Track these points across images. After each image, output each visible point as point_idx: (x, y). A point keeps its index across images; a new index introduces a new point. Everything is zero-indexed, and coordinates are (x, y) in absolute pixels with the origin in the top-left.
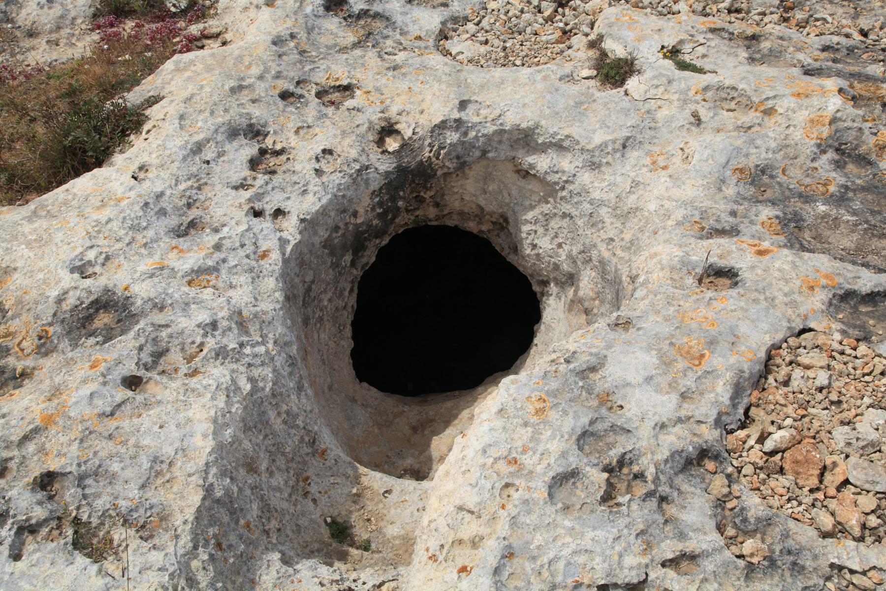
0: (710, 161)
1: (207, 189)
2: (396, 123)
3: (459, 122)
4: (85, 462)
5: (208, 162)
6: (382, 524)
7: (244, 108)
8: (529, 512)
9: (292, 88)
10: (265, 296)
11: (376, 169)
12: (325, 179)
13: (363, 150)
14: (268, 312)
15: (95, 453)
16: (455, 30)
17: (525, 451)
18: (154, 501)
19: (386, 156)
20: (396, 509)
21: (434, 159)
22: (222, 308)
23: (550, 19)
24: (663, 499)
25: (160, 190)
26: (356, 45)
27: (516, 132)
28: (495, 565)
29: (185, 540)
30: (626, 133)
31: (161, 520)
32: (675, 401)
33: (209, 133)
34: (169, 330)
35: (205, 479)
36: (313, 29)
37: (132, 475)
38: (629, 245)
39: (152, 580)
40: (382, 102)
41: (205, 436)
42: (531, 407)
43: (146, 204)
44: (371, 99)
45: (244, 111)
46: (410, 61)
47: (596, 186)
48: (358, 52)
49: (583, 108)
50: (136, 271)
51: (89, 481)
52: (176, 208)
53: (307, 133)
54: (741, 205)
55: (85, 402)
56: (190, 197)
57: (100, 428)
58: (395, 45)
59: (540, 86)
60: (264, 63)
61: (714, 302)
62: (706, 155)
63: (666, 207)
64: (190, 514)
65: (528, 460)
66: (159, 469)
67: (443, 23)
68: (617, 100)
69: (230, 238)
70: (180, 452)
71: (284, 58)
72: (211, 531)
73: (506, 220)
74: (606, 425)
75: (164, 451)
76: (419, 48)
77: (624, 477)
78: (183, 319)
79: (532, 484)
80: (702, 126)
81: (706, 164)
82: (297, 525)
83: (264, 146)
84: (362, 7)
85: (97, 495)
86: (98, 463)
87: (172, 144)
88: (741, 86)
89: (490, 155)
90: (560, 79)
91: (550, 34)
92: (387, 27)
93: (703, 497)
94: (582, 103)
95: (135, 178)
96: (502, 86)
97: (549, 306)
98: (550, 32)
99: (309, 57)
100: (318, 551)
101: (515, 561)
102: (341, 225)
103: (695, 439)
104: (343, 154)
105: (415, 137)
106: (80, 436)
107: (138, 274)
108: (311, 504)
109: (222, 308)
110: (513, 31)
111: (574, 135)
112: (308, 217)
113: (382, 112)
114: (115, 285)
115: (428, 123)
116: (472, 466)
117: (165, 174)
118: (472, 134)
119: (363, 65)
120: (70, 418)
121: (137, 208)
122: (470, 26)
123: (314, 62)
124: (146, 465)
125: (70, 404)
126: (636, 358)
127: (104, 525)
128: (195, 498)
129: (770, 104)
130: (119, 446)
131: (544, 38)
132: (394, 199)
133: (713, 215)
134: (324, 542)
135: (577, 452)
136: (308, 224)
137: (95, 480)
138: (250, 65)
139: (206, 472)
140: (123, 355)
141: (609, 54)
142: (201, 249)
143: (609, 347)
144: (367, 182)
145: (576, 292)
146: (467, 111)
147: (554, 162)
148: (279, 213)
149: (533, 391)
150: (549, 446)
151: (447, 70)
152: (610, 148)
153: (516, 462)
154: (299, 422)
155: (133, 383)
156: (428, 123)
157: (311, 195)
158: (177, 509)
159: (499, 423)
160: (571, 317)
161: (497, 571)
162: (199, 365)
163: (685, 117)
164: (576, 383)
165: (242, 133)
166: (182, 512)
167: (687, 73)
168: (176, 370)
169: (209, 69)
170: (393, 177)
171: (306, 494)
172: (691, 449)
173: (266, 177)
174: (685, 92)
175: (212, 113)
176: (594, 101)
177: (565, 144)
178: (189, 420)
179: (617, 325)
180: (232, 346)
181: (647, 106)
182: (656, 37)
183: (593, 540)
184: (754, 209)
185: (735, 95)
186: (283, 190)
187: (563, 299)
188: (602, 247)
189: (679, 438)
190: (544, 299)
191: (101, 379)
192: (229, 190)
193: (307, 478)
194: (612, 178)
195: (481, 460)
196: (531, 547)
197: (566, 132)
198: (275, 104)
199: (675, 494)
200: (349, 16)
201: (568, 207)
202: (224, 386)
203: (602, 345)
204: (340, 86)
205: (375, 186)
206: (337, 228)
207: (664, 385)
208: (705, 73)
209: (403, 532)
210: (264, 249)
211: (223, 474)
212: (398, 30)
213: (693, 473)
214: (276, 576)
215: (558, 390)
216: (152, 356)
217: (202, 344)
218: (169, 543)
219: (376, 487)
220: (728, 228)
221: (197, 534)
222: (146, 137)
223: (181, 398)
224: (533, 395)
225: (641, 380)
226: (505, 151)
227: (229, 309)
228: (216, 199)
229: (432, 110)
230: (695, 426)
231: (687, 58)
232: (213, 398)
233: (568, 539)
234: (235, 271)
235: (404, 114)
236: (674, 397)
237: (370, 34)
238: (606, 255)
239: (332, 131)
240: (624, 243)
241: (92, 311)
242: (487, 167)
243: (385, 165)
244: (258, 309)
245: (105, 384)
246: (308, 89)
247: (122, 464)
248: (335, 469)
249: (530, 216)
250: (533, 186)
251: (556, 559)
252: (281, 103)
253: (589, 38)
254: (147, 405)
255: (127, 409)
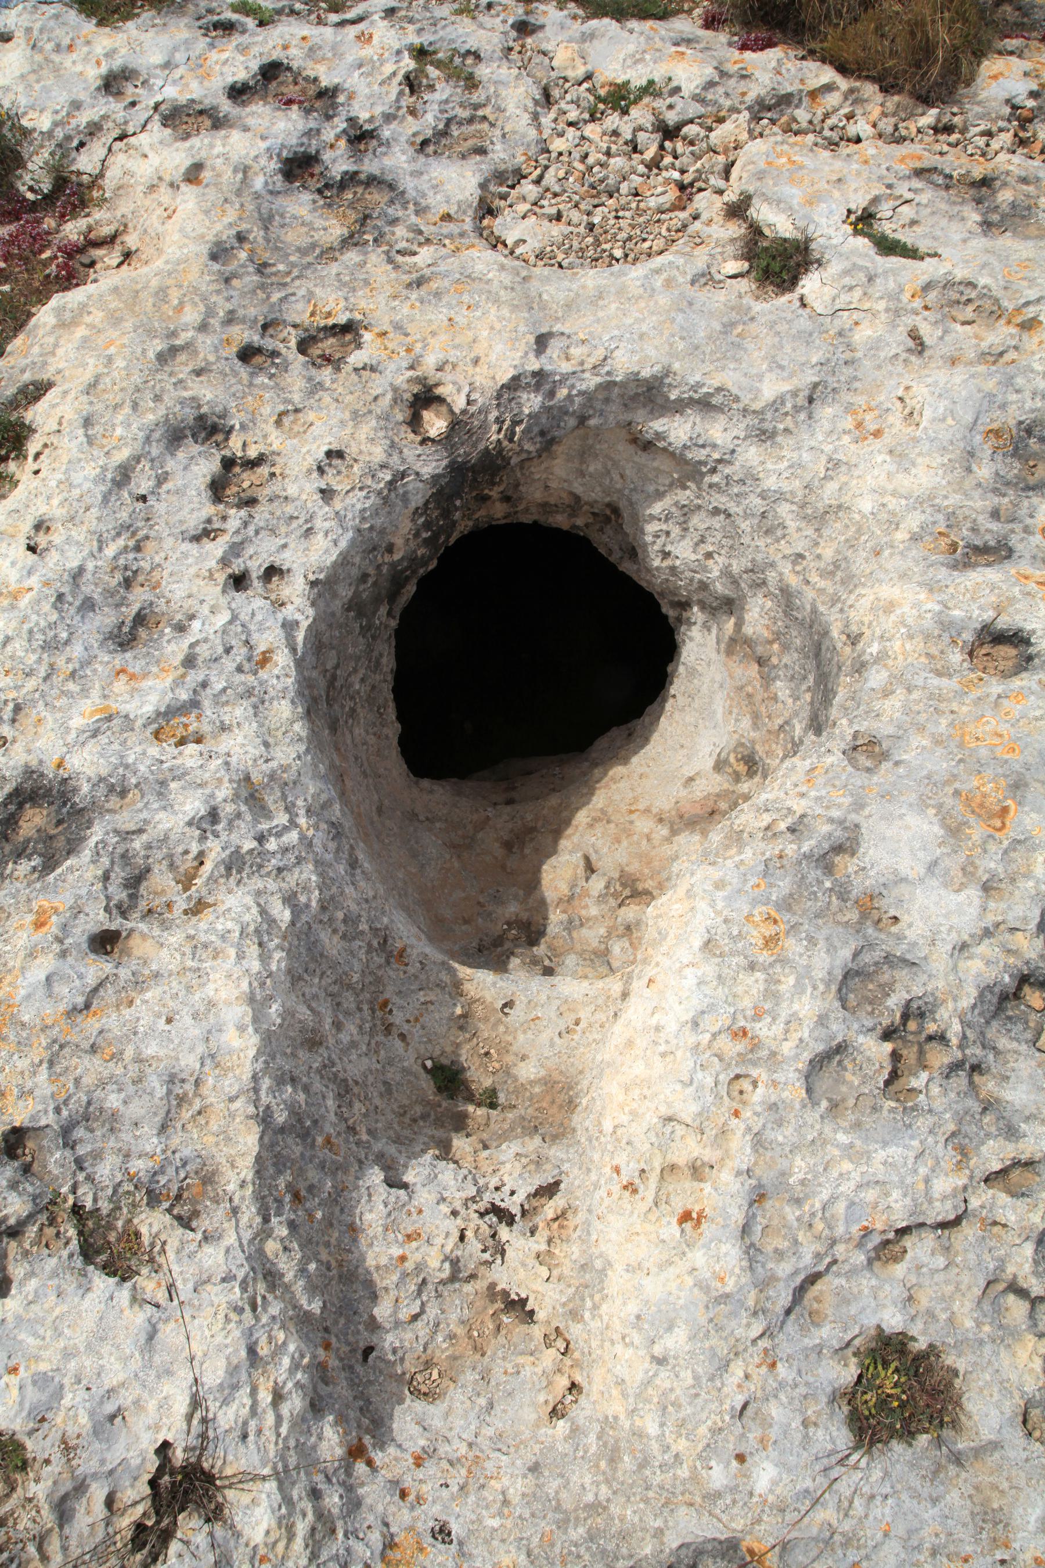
0: (950, 421)
1: (150, 546)
2: (437, 385)
3: (540, 375)
4: (66, 1102)
5: (143, 498)
6: (509, 1059)
7: (185, 389)
8: (780, 1123)
9: (256, 339)
10: (279, 734)
11: (417, 474)
12: (338, 504)
13: (393, 445)
14: (289, 766)
15: (77, 1081)
16: (504, 197)
17: (757, 1016)
18: (186, 1152)
19: (429, 448)
20: (525, 1032)
21: (505, 443)
22: (220, 780)
23: (654, 165)
24: (976, 1068)
25: (75, 564)
26: (349, 241)
27: (633, 385)
28: (741, 1222)
29: (249, 1214)
30: (810, 377)
31: (204, 1183)
32: (977, 902)
33: (138, 445)
34: (144, 837)
35: (256, 1103)
36: (271, 218)
37: (143, 1111)
38: (831, 568)
39: (216, 1301)
40: (409, 350)
41: (241, 1029)
42: (755, 933)
43: (60, 597)
44: (391, 346)
45: (186, 394)
46: (442, 268)
47: (772, 468)
48: (352, 256)
49: (735, 332)
50: (68, 730)
51: (79, 1133)
52: (109, 593)
53: (294, 422)
54: (1004, 495)
55: (41, 993)
56: (126, 568)
57: (74, 1038)
58: (411, 235)
59: (663, 300)
60: (204, 299)
61: (1005, 702)
62: (941, 410)
63: (890, 507)
64: (246, 1169)
65: (763, 1029)
66: (180, 1097)
67: (483, 186)
68: (789, 316)
69: (206, 640)
70: (208, 1061)
71: (235, 282)
72: (282, 1183)
73: (616, 510)
74: (878, 954)
75: (183, 1063)
76: (450, 236)
77: (910, 1037)
78: (162, 815)
79: (779, 1077)
80: (926, 354)
81: (943, 426)
82: (385, 1083)
83: (227, 453)
84: (345, 168)
85: (97, 1156)
86: (85, 1099)
87: (81, 474)
88: (982, 281)
89: (592, 422)
90: (693, 283)
91: (660, 194)
92: (392, 202)
93: (1033, 1057)
94: (733, 324)
95: (32, 549)
96: (601, 303)
97: (691, 639)
98: (660, 189)
99: (275, 274)
100: (424, 1117)
101: (768, 1204)
102: (371, 571)
103: (1011, 960)
104: (361, 458)
105: (473, 409)
106: (46, 1055)
107: (73, 734)
108: (398, 1044)
109: (220, 780)
110: (601, 191)
111: (729, 385)
112: (322, 576)
113: (412, 367)
114: (41, 762)
115: (491, 384)
116: (678, 1047)
117: (79, 534)
118: (562, 393)
119: (367, 283)
120: (23, 1025)
121: (46, 607)
122: (528, 188)
123: (285, 285)
124: (160, 1091)
125: (18, 999)
126: (908, 827)
127: (120, 1208)
128: (249, 1140)
129: (1030, 312)
130: (111, 1064)
131: (652, 203)
132: (446, 513)
133: (965, 518)
134: (428, 1103)
135: (841, 1013)
136: (322, 588)
137: (87, 1128)
138: (181, 304)
139: (256, 1090)
140: (80, 897)
141: (767, 231)
142: (163, 670)
143: (859, 806)
144: (405, 498)
145: (739, 625)
146: (549, 351)
147: (698, 429)
148: (272, 572)
149: (754, 902)
150: (796, 1007)
151: (506, 278)
152: (789, 405)
153: (745, 1033)
154: (364, 926)
155: (105, 942)
156: (491, 384)
157: (320, 536)
158: (224, 1161)
159: (709, 969)
160: (731, 664)
161: (745, 1230)
162: (204, 892)
163: (897, 341)
164: (820, 882)
165: (188, 433)
166: (233, 1166)
167: (895, 261)
168: (169, 905)
169: (115, 320)
170: (443, 482)
171: (388, 1029)
172: (1007, 979)
173: (243, 513)
174: (893, 297)
175: (135, 406)
176: (752, 319)
177: (714, 401)
178: (211, 1004)
179: (855, 748)
180: (249, 844)
181: (837, 322)
182: (836, 194)
183: (885, 1163)
184: (1026, 503)
185: (973, 295)
186: (273, 531)
187: (714, 631)
188: (786, 568)
189: (988, 963)
190: (683, 628)
191: (56, 947)
192: (186, 546)
193: (385, 1003)
194: (795, 455)
195: (692, 1039)
196: (791, 1181)
197: (716, 383)
198: (236, 374)
199: (991, 1057)
200: (327, 186)
201: (724, 499)
202: (252, 928)
203: (847, 801)
204: (335, 326)
205: (417, 501)
206: (364, 577)
207: (956, 873)
208: (922, 259)
209: (543, 1073)
210: (262, 648)
211: (280, 1081)
212: (411, 206)
213: (1010, 1013)
214: (385, 1211)
215: (791, 895)
216: (126, 886)
217: (201, 854)
218: (226, 1225)
219: (489, 999)
220: (992, 543)
221: (263, 1198)
222: (36, 467)
223: (190, 963)
224: (756, 912)
225: (922, 871)
226: (615, 414)
227: (231, 781)
228: (169, 567)
229: (493, 358)
230: (1007, 935)
231: (887, 228)
232: (240, 956)
233: (847, 1166)
234: (224, 699)
235: (448, 368)
236: (973, 893)
237: (366, 217)
238: (793, 581)
239: (339, 415)
240: (822, 565)
241: (12, 808)
242: (585, 438)
243: (430, 465)
244: (274, 764)
245: (63, 954)
246: (281, 336)
247: (123, 1095)
248: (423, 977)
249: (657, 508)
250: (661, 463)
251: (833, 1199)
252: (243, 371)
253: (726, 198)
254: (139, 983)
255: (109, 993)
